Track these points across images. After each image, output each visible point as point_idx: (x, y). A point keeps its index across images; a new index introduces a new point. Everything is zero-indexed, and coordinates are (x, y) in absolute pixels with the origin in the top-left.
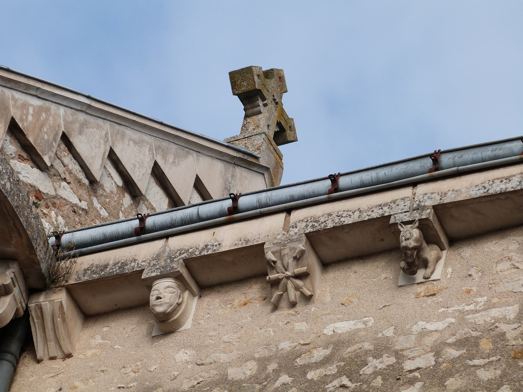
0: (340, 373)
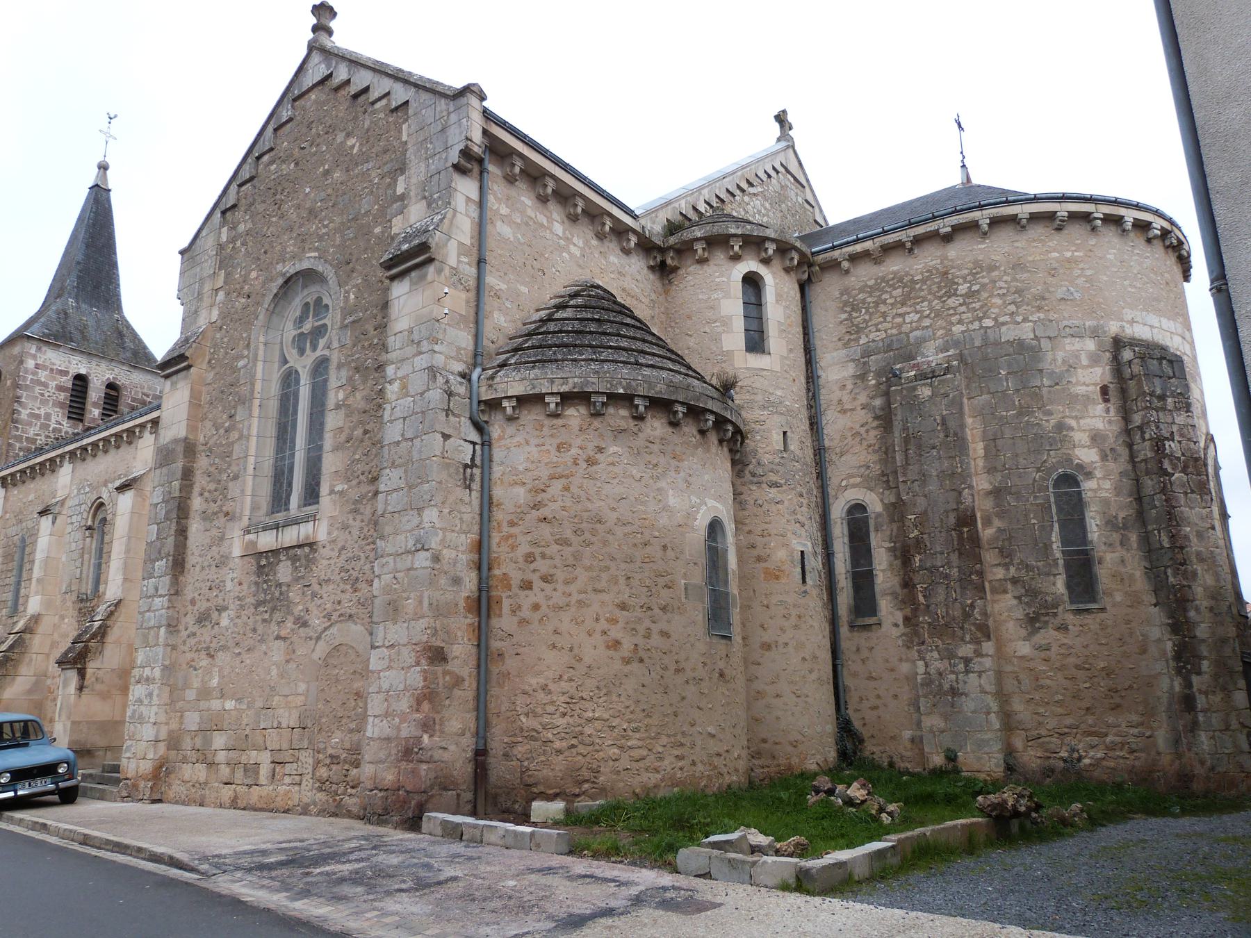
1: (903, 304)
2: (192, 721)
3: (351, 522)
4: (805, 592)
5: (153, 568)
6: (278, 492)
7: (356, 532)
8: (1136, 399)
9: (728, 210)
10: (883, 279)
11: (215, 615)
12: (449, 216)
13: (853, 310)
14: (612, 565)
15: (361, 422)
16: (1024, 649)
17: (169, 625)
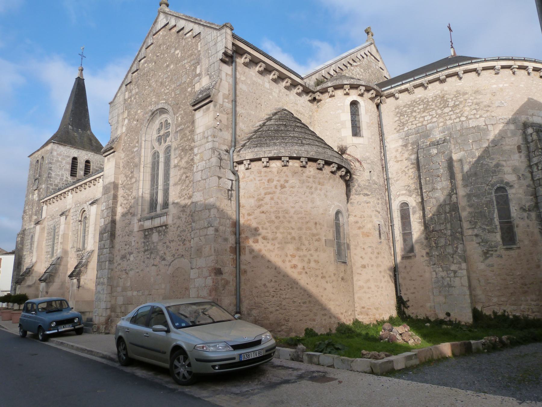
0: (421, 102)
1: (424, 112)
2: (120, 300)
3: (182, 215)
4: (381, 242)
5: (103, 237)
6: (152, 204)
7: (184, 220)
8: (534, 151)
9: (344, 73)
10: (414, 101)
11: (128, 256)
12: (219, 82)
13: (401, 115)
14: (293, 231)
15: (184, 173)
16: (482, 266)
17: (110, 261)
